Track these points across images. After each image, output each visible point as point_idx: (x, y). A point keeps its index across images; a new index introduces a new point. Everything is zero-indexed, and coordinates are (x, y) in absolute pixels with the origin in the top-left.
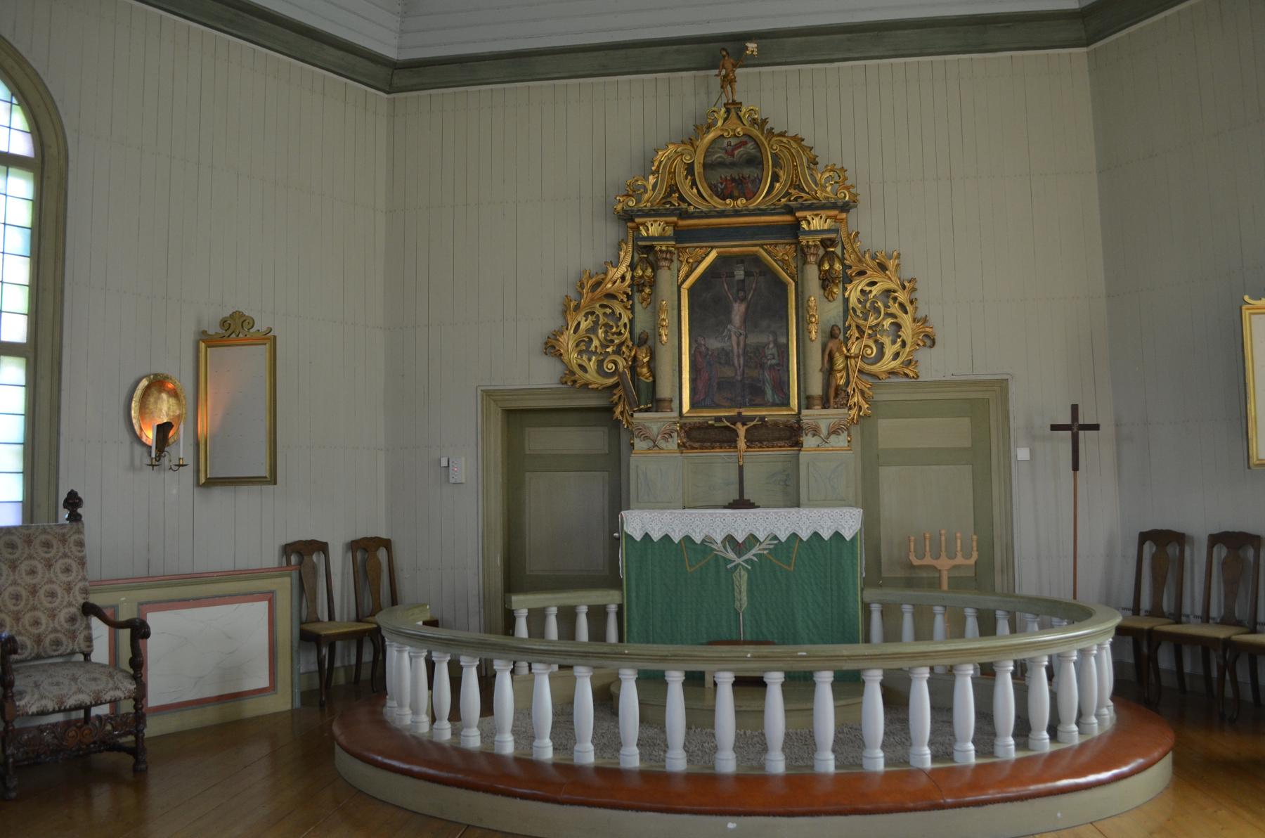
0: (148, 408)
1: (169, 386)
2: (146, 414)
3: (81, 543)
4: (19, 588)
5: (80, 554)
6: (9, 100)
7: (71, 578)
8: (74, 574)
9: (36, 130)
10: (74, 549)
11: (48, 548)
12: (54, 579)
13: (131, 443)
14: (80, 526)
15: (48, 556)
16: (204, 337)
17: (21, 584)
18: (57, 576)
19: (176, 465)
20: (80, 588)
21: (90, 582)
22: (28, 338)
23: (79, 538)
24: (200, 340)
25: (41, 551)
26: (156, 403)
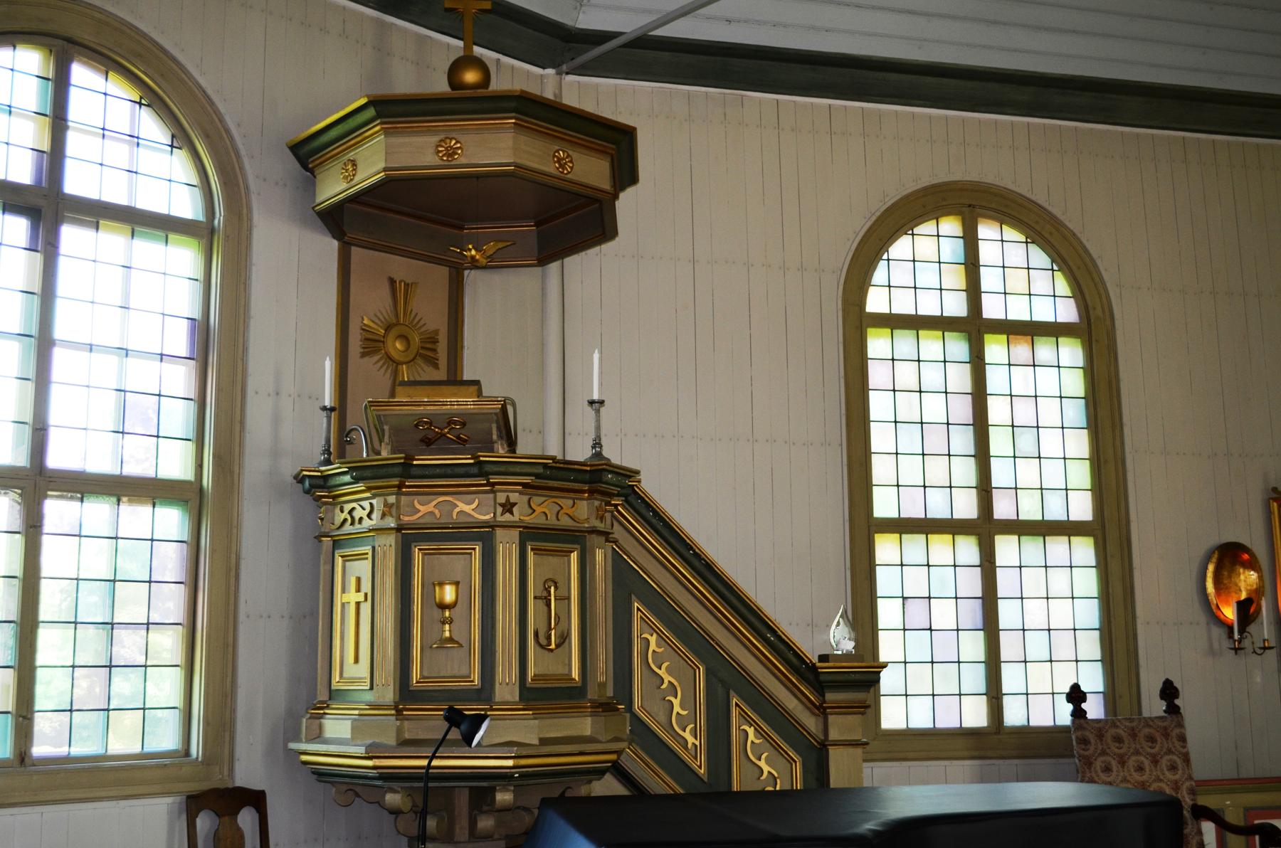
0: (1222, 583)
1: (1243, 556)
2: (1222, 589)
3: (1085, 740)
4: (1163, 785)
5: (1184, 751)
6: (1050, 268)
7: (1177, 777)
8: (1180, 772)
9: (1079, 294)
10: (1177, 744)
11: (1086, 745)
12: (1162, 777)
13: (1208, 624)
14: (1180, 719)
15: (1121, 751)
16: (1275, 496)
17: (1130, 782)
18: (1164, 774)
19: (1260, 648)
20: (1187, 788)
21: (1196, 781)
22: (1094, 516)
23: (1181, 732)
24: (1270, 498)
25: (1146, 745)
26: (1230, 577)
